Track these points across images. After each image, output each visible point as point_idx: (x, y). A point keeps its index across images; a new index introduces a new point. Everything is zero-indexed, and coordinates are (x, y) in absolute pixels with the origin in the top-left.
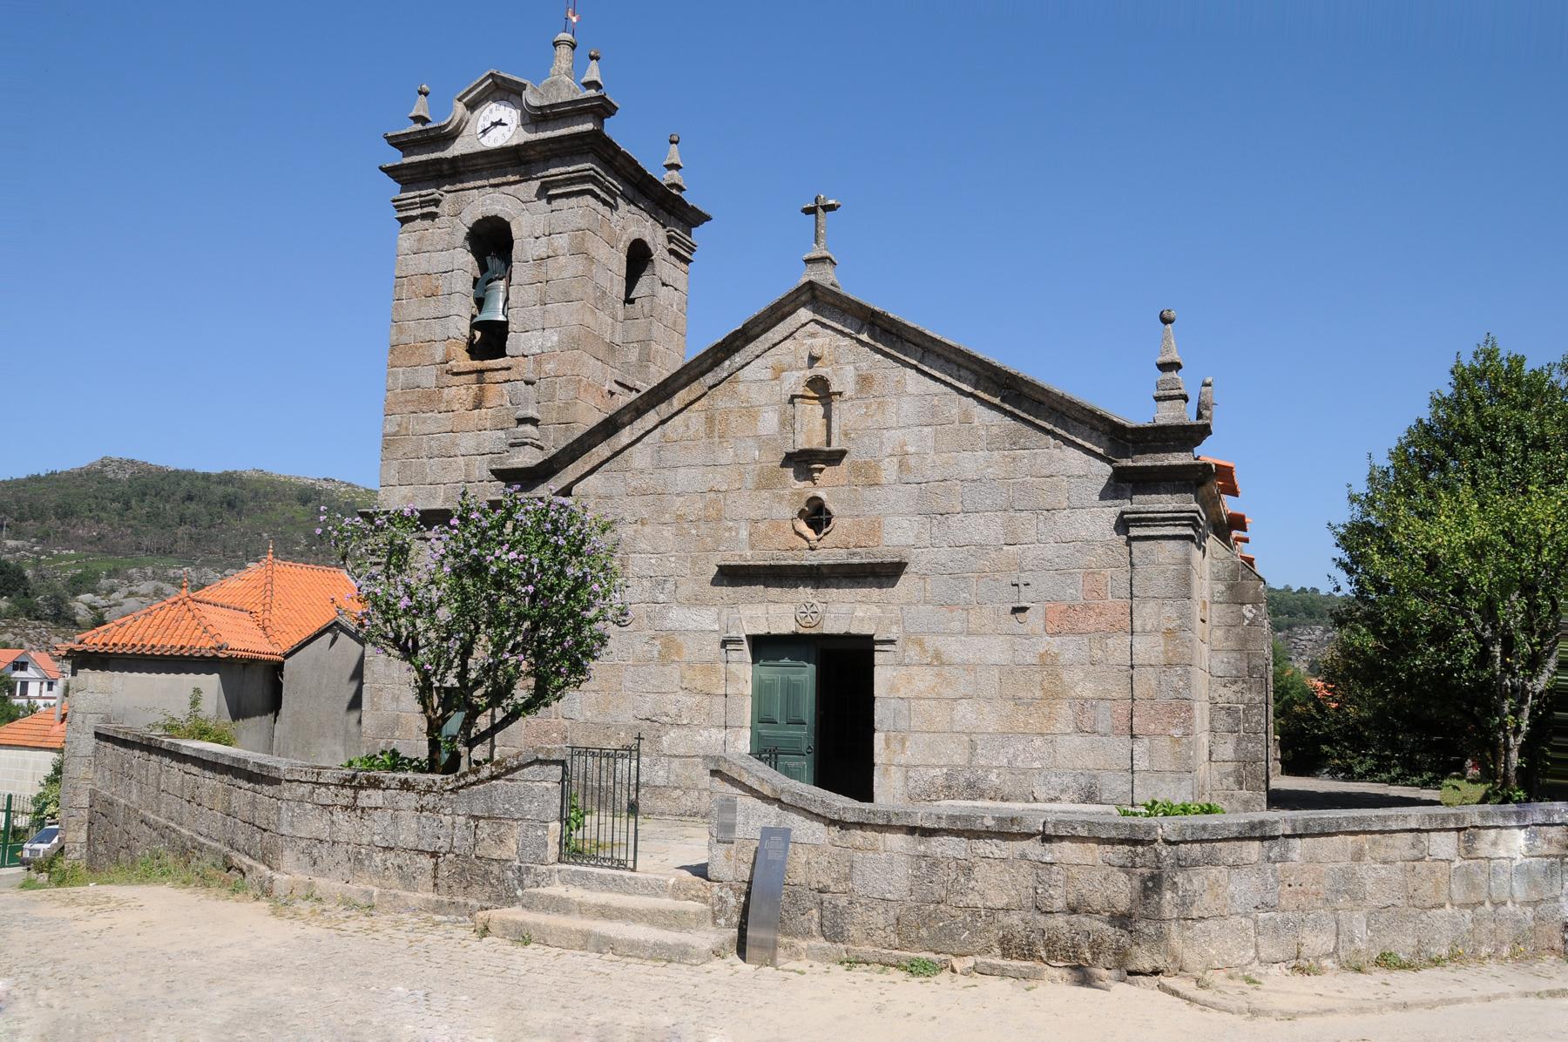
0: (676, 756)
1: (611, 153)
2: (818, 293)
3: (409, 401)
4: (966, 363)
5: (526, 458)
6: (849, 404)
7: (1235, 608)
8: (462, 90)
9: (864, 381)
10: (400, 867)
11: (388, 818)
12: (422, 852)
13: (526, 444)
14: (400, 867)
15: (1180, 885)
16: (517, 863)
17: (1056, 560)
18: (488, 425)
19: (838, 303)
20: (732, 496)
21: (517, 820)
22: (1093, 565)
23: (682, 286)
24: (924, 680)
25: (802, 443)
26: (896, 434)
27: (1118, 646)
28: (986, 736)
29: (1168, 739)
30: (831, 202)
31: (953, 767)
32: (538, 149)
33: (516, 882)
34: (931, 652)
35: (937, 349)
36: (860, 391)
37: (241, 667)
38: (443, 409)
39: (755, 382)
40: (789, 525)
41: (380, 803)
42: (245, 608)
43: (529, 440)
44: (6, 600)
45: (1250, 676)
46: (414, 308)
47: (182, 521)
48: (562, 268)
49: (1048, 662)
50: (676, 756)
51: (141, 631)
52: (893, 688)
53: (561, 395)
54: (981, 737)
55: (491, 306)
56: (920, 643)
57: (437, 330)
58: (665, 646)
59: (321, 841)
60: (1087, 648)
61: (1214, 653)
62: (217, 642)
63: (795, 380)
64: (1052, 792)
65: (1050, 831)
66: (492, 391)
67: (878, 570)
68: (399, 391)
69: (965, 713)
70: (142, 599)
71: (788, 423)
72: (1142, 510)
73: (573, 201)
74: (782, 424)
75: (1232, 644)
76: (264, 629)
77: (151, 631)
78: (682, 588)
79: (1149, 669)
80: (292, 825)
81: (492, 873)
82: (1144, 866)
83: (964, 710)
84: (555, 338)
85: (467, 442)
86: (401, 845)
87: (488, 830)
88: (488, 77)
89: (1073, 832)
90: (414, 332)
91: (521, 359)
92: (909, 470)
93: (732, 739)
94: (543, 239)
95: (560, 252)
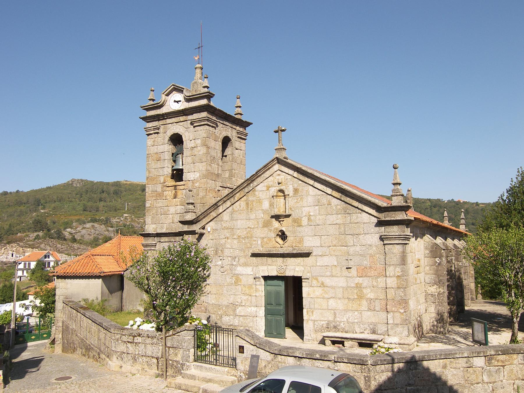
0: (241, 316)
1: (213, 110)
2: (279, 161)
3: (153, 196)
4: (328, 185)
5: (189, 217)
6: (291, 198)
7: (433, 259)
8: (164, 91)
9: (296, 191)
10: (147, 362)
11: (143, 346)
12: (153, 357)
13: (190, 212)
14: (147, 362)
15: (377, 379)
16: (181, 362)
17: (360, 251)
18: (179, 204)
19: (286, 164)
20: (255, 230)
21: (181, 348)
22: (373, 253)
23: (243, 148)
24: (318, 292)
25: (276, 212)
26: (307, 209)
27: (381, 282)
28: (339, 311)
29: (399, 313)
30: (283, 128)
31: (329, 321)
32: (189, 110)
33: (181, 368)
34: (321, 282)
35: (318, 180)
36: (295, 194)
37: (109, 277)
38: (164, 198)
39: (261, 191)
40: (273, 239)
41: (141, 342)
42: (111, 254)
43: (191, 211)
44: (42, 232)
45: (439, 283)
46: (153, 165)
47: (101, 200)
48: (199, 151)
49: (358, 286)
50: (241, 316)
51: (76, 267)
52: (309, 294)
53: (201, 194)
54: (338, 311)
55: (178, 163)
56: (317, 279)
57: (161, 172)
58: (236, 279)
59: (124, 353)
60: (371, 282)
61: (426, 275)
62: (100, 270)
63: (273, 191)
64: (361, 330)
65: (336, 360)
66: (179, 193)
67: (302, 255)
68: (150, 192)
69: (332, 303)
70: (87, 230)
71: (271, 205)
72: (388, 235)
73: (202, 127)
74: (270, 206)
75: (432, 272)
76: (117, 262)
77: (79, 267)
78: (241, 260)
79: (392, 289)
80: (115, 347)
81: (174, 365)
82: (365, 372)
83: (332, 302)
84: (198, 175)
85: (172, 210)
86: (147, 355)
87: (173, 351)
88: (172, 86)
89: (343, 361)
90: (154, 173)
91: (188, 182)
92: (311, 221)
93: (258, 311)
94: (193, 141)
95: (198, 145)
